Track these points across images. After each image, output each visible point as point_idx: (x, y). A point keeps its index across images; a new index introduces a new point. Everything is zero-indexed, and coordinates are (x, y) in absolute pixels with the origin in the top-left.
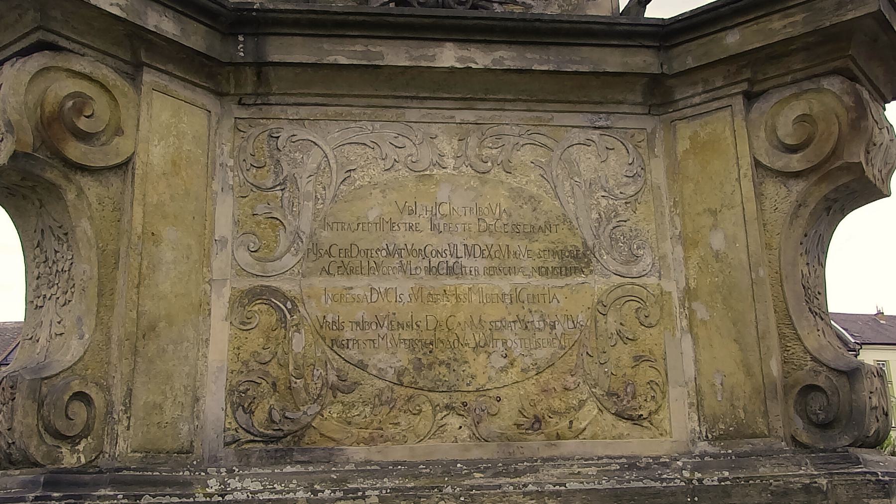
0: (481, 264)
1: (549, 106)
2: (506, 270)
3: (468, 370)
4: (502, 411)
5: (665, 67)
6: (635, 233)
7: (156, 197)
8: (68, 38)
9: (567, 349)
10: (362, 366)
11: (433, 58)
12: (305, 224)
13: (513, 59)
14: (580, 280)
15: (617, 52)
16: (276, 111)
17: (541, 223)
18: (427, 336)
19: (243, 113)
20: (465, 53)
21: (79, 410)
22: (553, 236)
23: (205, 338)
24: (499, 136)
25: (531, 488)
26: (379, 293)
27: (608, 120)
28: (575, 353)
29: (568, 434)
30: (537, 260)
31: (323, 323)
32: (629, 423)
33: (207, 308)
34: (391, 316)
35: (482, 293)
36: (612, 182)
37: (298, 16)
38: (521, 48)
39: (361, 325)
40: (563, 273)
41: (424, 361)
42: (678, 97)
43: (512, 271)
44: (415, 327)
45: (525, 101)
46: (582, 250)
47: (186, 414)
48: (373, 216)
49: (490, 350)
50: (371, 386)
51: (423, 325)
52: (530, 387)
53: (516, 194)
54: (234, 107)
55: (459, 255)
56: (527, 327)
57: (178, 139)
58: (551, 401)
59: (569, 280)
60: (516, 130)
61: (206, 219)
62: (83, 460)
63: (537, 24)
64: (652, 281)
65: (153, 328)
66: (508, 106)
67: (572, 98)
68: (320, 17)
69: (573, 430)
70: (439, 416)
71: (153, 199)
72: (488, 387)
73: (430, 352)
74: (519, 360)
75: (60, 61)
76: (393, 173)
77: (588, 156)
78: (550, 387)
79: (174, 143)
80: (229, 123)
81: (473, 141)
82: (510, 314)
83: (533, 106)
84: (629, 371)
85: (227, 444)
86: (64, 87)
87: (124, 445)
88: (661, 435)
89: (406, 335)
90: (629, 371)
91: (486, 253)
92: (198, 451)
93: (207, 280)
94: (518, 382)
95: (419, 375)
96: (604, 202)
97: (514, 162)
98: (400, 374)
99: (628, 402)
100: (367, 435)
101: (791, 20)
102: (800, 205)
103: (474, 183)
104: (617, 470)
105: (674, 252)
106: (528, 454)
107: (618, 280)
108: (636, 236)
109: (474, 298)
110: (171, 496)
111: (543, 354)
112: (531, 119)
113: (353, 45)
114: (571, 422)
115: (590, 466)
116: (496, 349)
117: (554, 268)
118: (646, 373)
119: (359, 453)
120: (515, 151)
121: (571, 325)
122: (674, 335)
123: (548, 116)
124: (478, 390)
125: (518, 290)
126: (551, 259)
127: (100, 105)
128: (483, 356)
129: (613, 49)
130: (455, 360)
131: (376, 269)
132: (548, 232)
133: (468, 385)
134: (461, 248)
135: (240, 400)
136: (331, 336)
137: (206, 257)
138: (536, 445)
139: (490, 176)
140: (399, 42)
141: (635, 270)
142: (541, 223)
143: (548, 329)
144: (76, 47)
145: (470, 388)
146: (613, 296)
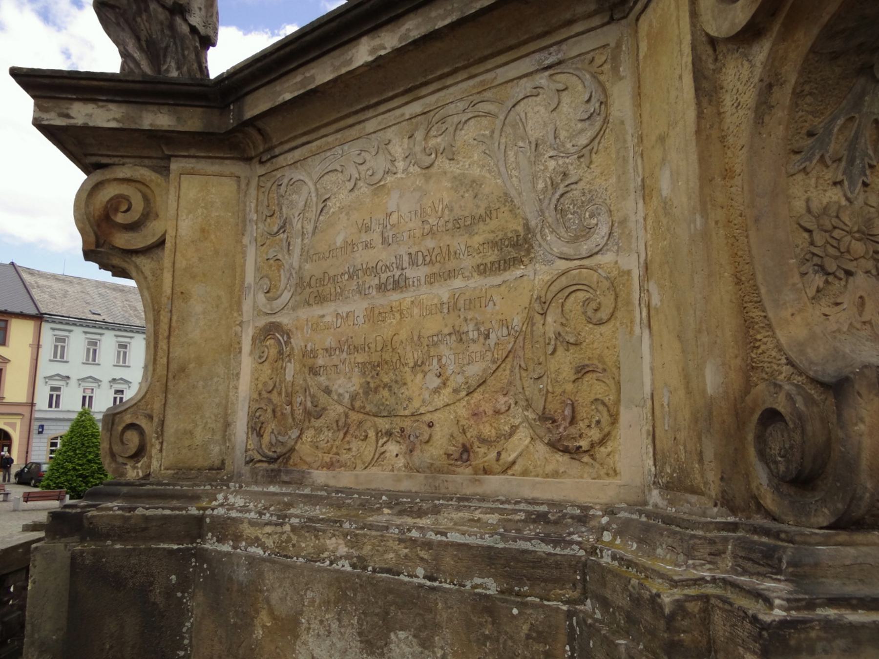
0: (422, 272)
1: (490, 64)
2: (446, 275)
3: (407, 393)
4: (435, 438)
6: (589, 196)
7: (184, 262)
8: (108, 156)
9: (499, 362)
10: (328, 391)
12: (295, 260)
14: (519, 273)
17: (482, 211)
18: (375, 358)
20: (377, 42)
22: (493, 224)
23: (235, 372)
24: (443, 120)
25: (414, 534)
26: (342, 318)
27: (559, 51)
28: (508, 367)
29: (497, 467)
30: (476, 257)
32: (566, 458)
33: (237, 346)
34: (350, 340)
36: (563, 134)
37: (250, 70)
40: (502, 268)
41: (372, 385)
43: (450, 275)
44: (367, 349)
45: (465, 67)
46: (522, 234)
47: (218, 437)
49: (426, 368)
50: (336, 411)
51: (373, 346)
52: (462, 410)
53: (460, 182)
54: (258, 166)
55: (404, 266)
56: (461, 339)
57: (206, 209)
58: (481, 427)
60: (461, 105)
61: (234, 270)
62: (141, 474)
64: (606, 259)
65: (182, 369)
66: (449, 81)
67: (512, 41)
68: (264, 62)
69: (501, 462)
70: (381, 442)
71: (181, 263)
72: (422, 411)
73: (377, 374)
74: (452, 378)
75: (108, 174)
76: (356, 192)
77: (536, 109)
78: (481, 409)
79: (202, 213)
81: (419, 135)
82: (446, 326)
83: (473, 70)
84: (569, 387)
85: (247, 463)
86: (110, 192)
87: (158, 461)
88: (608, 474)
90: (569, 387)
91: (428, 259)
92: (229, 467)
93: (237, 323)
94: (448, 405)
95: (367, 399)
96: (552, 164)
97: (459, 144)
98: (353, 398)
99: (565, 428)
100: (328, 460)
104: (520, 521)
105: (633, 208)
106: (452, 488)
107: (563, 265)
108: (591, 200)
109: (416, 311)
110: (163, 508)
111: (475, 370)
112: (474, 87)
113: (295, 77)
114: (499, 454)
115: (492, 511)
116: (431, 367)
117: (492, 263)
118: (593, 388)
119: (320, 476)
120: (458, 132)
121: (505, 332)
122: (631, 332)
123: (489, 76)
124: (413, 415)
125: (456, 296)
126: (491, 252)
128: (420, 376)
130: (396, 382)
131: (340, 295)
132: (488, 220)
133: (405, 409)
134: (406, 258)
135: (256, 428)
138: (461, 480)
139: (434, 170)
140: (325, 59)
141: (585, 248)
142: (482, 211)
143: (482, 339)
144: (116, 160)
145: (407, 413)
146: (555, 288)
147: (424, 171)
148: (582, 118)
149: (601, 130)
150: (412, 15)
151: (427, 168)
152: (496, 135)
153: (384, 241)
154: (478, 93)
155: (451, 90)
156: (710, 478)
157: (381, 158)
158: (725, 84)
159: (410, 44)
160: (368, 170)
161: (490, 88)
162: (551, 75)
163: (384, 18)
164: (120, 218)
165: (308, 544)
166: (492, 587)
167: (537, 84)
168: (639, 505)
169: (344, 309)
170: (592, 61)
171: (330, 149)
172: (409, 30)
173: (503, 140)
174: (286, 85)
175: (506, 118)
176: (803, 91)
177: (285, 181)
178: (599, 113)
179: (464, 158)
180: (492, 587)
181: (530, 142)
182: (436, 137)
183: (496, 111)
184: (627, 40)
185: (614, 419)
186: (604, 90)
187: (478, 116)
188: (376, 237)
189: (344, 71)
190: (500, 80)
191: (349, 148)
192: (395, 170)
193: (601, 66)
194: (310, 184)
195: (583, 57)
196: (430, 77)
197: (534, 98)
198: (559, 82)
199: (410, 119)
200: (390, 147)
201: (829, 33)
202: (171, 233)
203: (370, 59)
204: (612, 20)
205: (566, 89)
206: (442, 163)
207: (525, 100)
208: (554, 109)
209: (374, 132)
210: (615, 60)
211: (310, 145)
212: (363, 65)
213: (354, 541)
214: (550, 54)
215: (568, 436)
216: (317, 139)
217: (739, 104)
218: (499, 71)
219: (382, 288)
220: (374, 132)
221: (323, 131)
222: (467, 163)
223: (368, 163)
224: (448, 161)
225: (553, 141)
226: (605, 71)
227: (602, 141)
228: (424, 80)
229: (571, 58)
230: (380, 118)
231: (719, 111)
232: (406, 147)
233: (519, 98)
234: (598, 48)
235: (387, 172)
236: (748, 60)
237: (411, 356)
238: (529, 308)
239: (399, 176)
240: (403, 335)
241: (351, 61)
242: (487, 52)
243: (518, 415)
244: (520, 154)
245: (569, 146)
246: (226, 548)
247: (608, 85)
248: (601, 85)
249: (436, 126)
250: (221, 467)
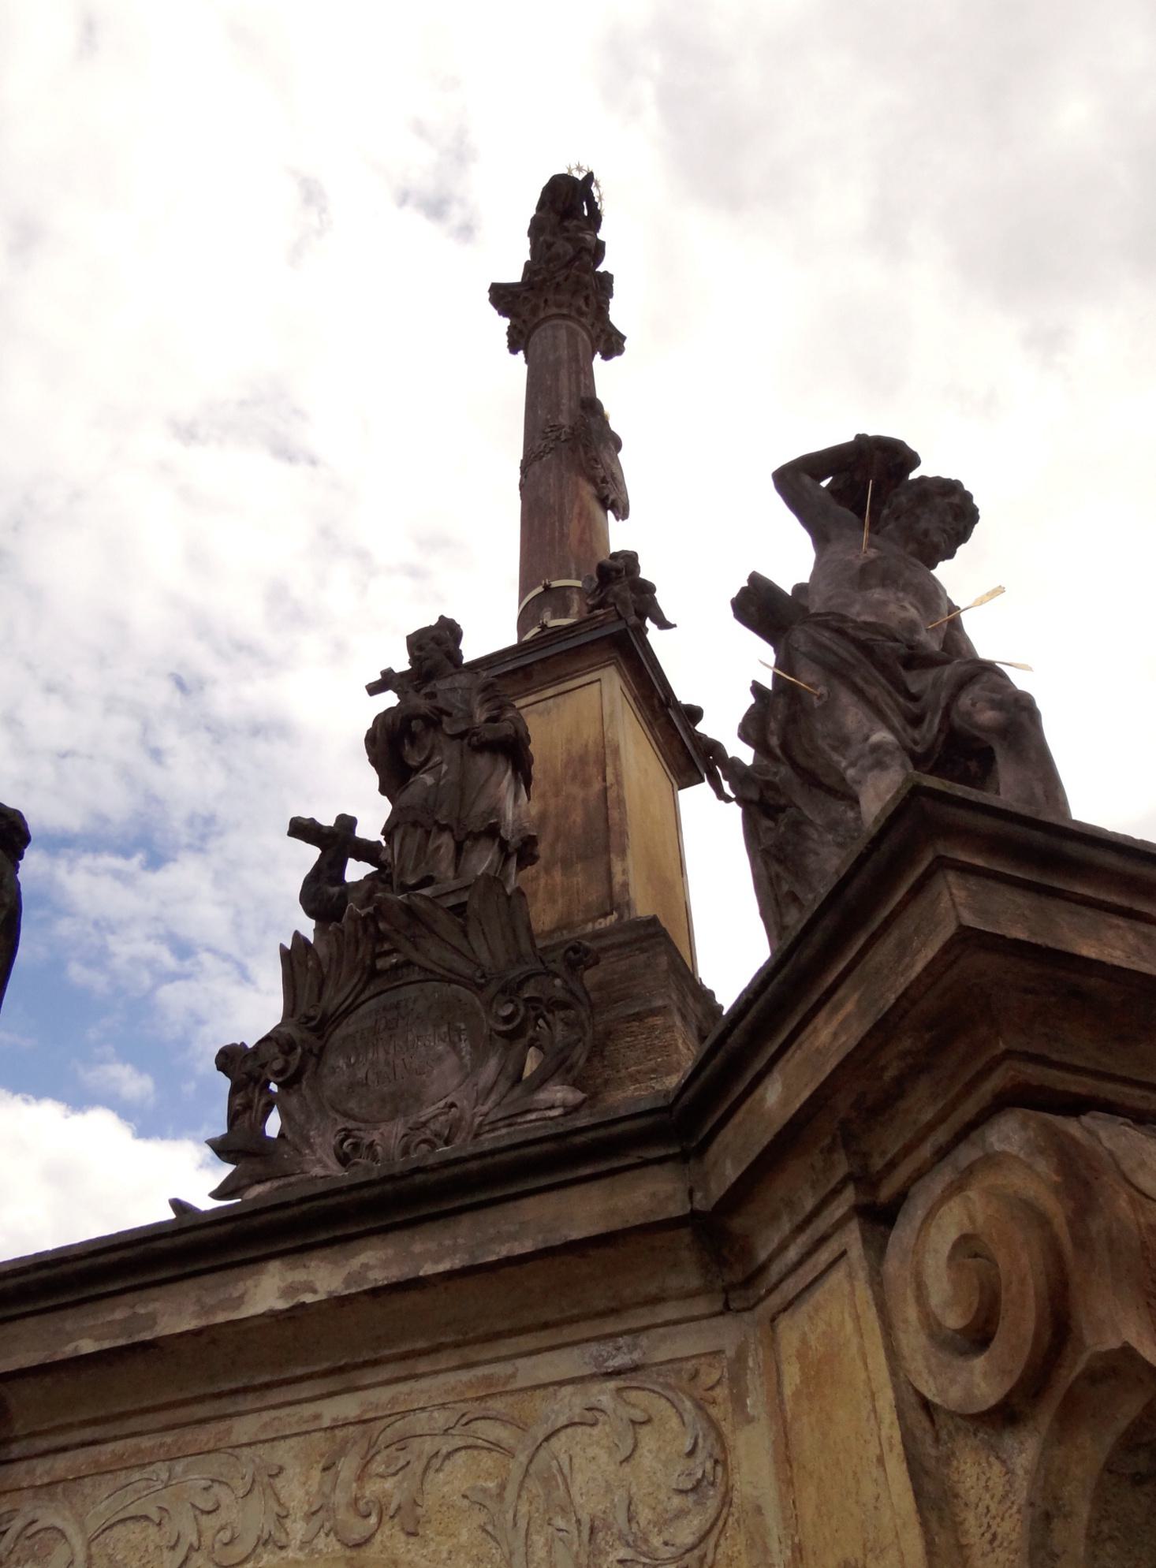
1: (505, 1347)
5: (698, 1195)
13: (385, 1264)
15: (595, 1190)
20: (299, 1276)
24: (402, 1442)
27: (634, 1347)
36: (645, 1515)
37: (21, 1279)
38: (405, 1235)
42: (763, 1256)
45: (457, 1345)
60: (441, 1418)
63: (419, 1178)
66: (423, 1365)
67: (551, 1315)
77: (592, 1451)
81: (348, 1467)
97: (430, 1501)
101: (840, 1016)
102: (1048, 1517)
112: (470, 1385)
113: (113, 1310)
120: (431, 1474)
129: (583, 1187)
140: (186, 1285)
147: (348, 1553)
148: (681, 1487)
149: (717, 1519)
150: (374, 1240)
151: (358, 1546)
152: (510, 1493)
154: (477, 1399)
155: (424, 1384)
157: (256, 1502)
158: (961, 1489)
159: (365, 1292)
160: (222, 1528)
161: (501, 1394)
162: (619, 1390)
163: (323, 1236)
167: (593, 1402)
170: (695, 1376)
171: (143, 1466)
172: (366, 1267)
173: (524, 1509)
174: (89, 1322)
175: (531, 1462)
176: (1100, 1532)
177: (17, 1524)
179: (439, 1534)
181: (578, 1521)
182: (382, 1476)
183: (512, 1442)
184: (756, 1350)
186: (720, 1437)
187: (476, 1447)
189: (221, 1318)
190: (519, 1383)
191: (185, 1472)
192: (283, 1540)
193: (712, 1388)
194: (78, 1542)
195: (676, 1366)
196: (387, 1352)
197: (588, 1429)
198: (634, 1406)
199: (332, 1428)
200: (279, 1483)
201: (1128, 1443)
203: (281, 1305)
204: (727, 1309)
205: (648, 1421)
207: (569, 1430)
208: (627, 1459)
209: (249, 1445)
210: (736, 1380)
211: (98, 1448)
212: (263, 1315)
214: (618, 1349)
216: (116, 1438)
217: (994, 1536)
218: (521, 1363)
220: (249, 1445)
221: (134, 1424)
222: (445, 1548)
223: (222, 1512)
224: (403, 1537)
225: (624, 1527)
226: (720, 1400)
227: (722, 1541)
228: (375, 1356)
229: (656, 1364)
230: (267, 1416)
231: (958, 1540)
232: (314, 1489)
233: (559, 1425)
234: (704, 1355)
235: (265, 1542)
236: (998, 1458)
239: (290, 1554)
241: (240, 1301)
242: (503, 1325)
244: (558, 1545)
245: (656, 1541)
247: (726, 1427)
248: (713, 1424)
249: (385, 1453)
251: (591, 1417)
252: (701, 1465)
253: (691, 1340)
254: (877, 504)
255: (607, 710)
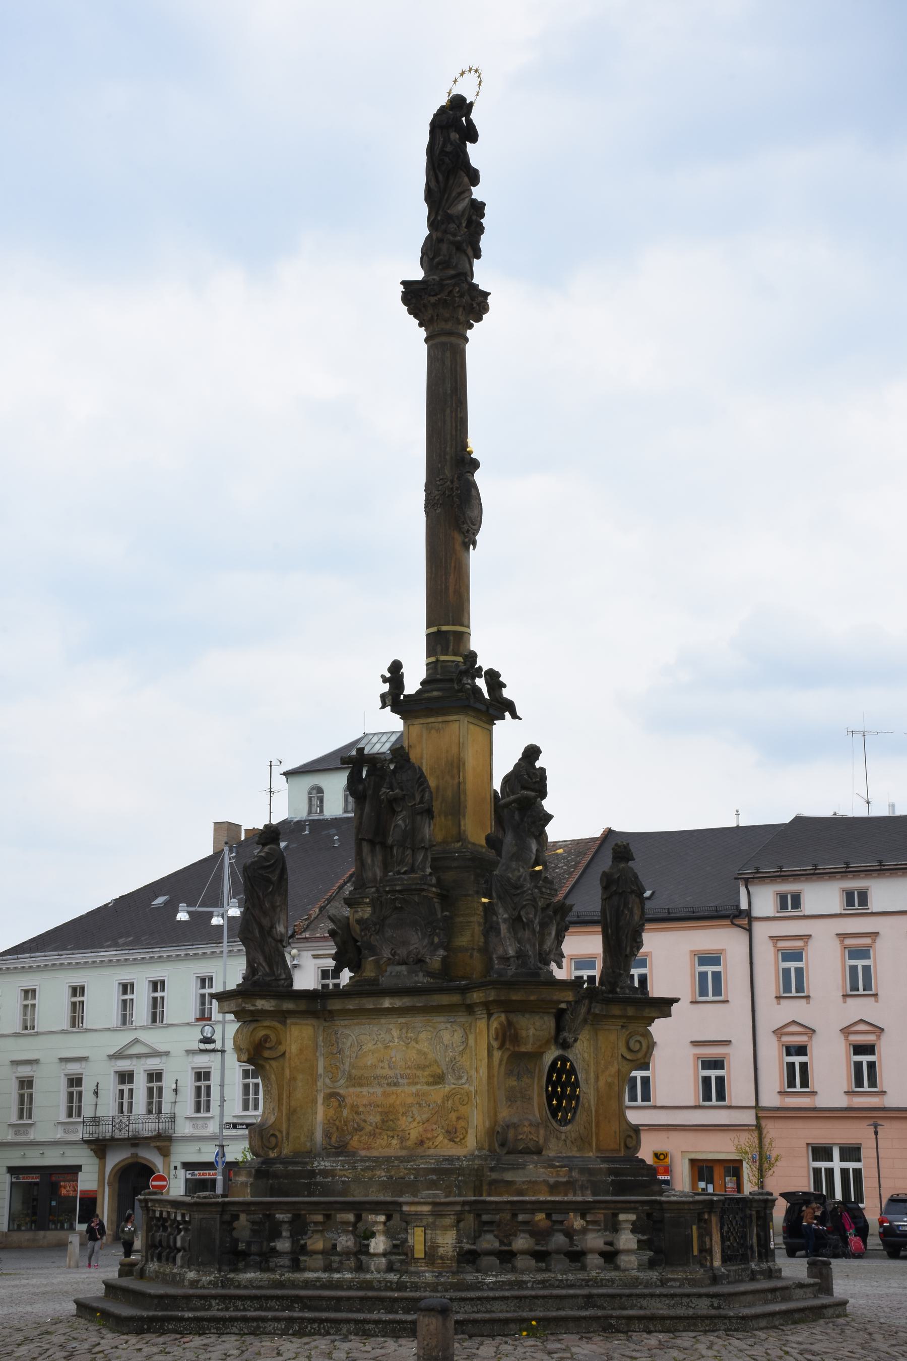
10: (365, 1121)
11: (382, 1004)
12: (347, 1067)
16: (337, 1022)
19: (327, 1024)
21: (273, 1140)
31: (352, 1106)
35: (406, 1093)
39: (365, 1106)
43: (416, 1083)
48: (369, 1063)
50: (369, 1128)
52: (421, 1129)
53: (419, 1052)
59: (436, 1087)
64: (466, 1086)
65: (295, 1111)
75: (259, 1024)
80: (321, 1028)
81: (404, 1031)
86: (261, 1033)
87: (286, 1151)
89: (379, 1110)
103: (404, 1048)
107: (454, 1086)
111: (425, 1116)
118: (462, 1123)
119: (363, 1153)
127: (273, 1037)
131: (369, 1085)
135: (327, 1135)
136: (355, 1110)
137: (315, 1082)
138: (420, 1151)
153: (390, 1067)
156: (486, 1146)
164: (267, 1045)
165: (369, 1174)
166: (434, 1177)
168: (472, 1155)
169: (371, 1090)
178: (465, 1041)
180: (434, 1177)
185: (467, 1132)
188: (386, 1064)
202: (288, 1051)
206: (413, 1044)
210: (470, 1027)
213: (388, 1171)
215: (452, 1135)
219: (389, 1084)
237: (401, 1110)
238: (443, 1098)
240: (398, 1102)
243: (439, 1130)
246: (329, 1179)
250: (311, 1152)
251: (446, 1029)
252: (464, 1039)
253: (463, 1019)
254: (532, 753)
255: (461, 740)
